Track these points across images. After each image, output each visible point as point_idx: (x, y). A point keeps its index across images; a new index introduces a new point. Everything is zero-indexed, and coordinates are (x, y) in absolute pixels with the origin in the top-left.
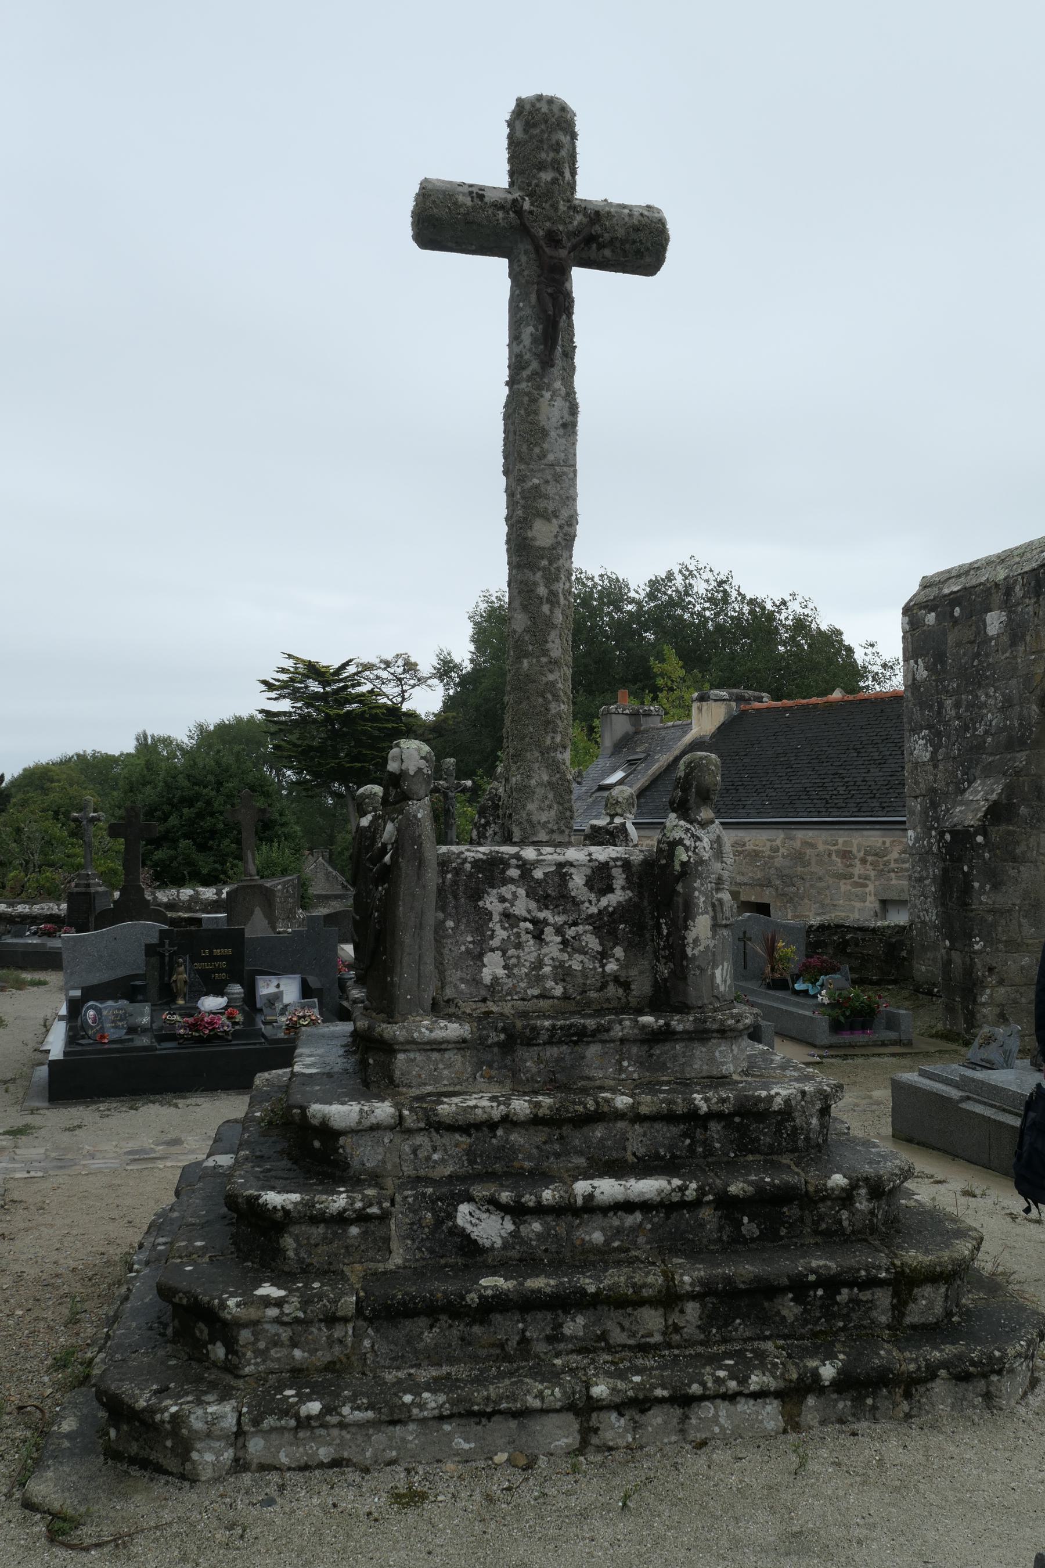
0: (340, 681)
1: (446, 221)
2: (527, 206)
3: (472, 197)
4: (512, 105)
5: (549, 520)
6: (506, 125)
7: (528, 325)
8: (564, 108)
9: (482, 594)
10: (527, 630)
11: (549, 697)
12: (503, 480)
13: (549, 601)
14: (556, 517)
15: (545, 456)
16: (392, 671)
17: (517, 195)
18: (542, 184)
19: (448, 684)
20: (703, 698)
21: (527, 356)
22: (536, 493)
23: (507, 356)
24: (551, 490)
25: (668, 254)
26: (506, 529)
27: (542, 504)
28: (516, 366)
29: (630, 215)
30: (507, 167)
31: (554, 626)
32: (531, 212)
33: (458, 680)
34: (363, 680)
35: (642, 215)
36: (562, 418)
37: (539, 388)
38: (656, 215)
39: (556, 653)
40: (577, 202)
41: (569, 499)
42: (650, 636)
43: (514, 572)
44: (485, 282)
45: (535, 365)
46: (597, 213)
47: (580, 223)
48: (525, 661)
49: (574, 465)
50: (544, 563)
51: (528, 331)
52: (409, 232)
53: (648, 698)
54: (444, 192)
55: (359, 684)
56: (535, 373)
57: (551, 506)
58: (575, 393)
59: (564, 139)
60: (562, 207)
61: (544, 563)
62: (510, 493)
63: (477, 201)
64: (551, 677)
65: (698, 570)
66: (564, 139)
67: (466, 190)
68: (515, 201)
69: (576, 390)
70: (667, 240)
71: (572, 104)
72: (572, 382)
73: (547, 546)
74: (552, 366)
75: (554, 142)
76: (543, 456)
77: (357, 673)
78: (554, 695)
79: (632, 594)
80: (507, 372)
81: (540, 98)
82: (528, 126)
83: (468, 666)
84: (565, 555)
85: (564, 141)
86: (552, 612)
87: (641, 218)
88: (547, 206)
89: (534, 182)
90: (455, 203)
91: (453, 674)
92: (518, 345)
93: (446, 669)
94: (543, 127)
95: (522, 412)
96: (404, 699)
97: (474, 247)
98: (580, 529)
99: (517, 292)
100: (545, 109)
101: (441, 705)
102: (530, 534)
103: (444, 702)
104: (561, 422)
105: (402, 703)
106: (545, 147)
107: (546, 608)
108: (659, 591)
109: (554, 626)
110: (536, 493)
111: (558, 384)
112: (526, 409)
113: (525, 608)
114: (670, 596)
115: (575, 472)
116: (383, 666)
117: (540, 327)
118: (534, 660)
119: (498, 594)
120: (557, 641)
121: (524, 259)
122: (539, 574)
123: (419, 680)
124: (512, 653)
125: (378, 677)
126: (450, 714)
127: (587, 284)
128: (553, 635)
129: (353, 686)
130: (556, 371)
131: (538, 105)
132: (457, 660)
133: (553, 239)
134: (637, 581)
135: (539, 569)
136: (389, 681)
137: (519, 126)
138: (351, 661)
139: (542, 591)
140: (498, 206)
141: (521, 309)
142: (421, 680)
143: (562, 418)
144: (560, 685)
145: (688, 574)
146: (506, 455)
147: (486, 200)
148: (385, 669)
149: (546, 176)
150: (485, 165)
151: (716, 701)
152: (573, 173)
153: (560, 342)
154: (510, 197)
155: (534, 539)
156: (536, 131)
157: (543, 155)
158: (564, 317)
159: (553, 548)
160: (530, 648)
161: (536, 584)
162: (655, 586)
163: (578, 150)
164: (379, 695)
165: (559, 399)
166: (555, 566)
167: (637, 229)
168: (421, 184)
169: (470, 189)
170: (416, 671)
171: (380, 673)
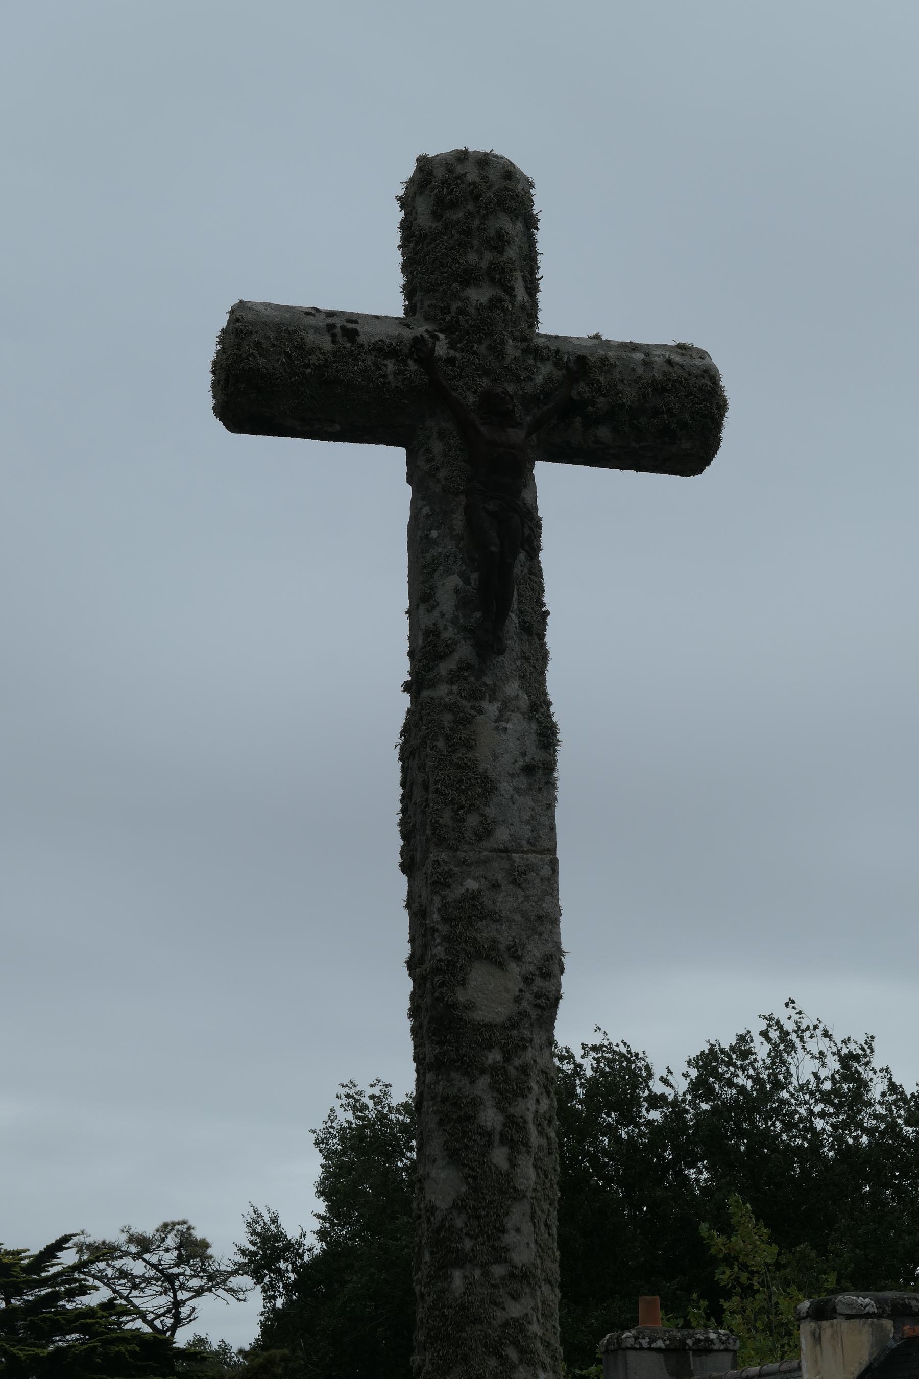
0: (44, 1283)
1: (278, 377)
2: (441, 349)
3: (334, 336)
4: (409, 170)
5: (501, 966)
6: (396, 205)
7: (448, 572)
8: (510, 173)
9: (343, 1091)
10: (458, 1206)
11: (513, 1354)
12: (403, 882)
13: (505, 1140)
14: (518, 958)
15: (489, 833)
16: (154, 1260)
17: (421, 329)
18: (472, 310)
19: (272, 1286)
20: (822, 1313)
21: (449, 634)
22: (473, 909)
23: (407, 632)
24: (505, 901)
25: (725, 434)
26: (408, 985)
27: (486, 932)
28: (426, 652)
29: (647, 364)
30: (400, 280)
31: (519, 1196)
32: (451, 361)
33: (293, 1276)
34: (91, 1281)
35: (669, 362)
36: (524, 754)
37: (475, 696)
38: (698, 362)
39: (523, 1256)
40: (541, 341)
41: (546, 920)
42: (699, 1175)
43: (429, 1077)
44: (359, 495)
45: (464, 650)
46: (582, 360)
47: (549, 379)
48: (457, 1274)
49: (552, 850)
50: (494, 1056)
51: (449, 585)
52: (208, 401)
53: (696, 1313)
54: (278, 327)
55: (83, 1290)
56: (465, 666)
57: (505, 936)
58: (549, 704)
59: (513, 229)
60: (512, 350)
61: (494, 1056)
62: (417, 908)
63: (342, 341)
64: (515, 1310)
65: (800, 1031)
66: (513, 229)
67: (321, 322)
68: (417, 341)
69: (551, 698)
70: (721, 407)
71: (525, 165)
72: (542, 682)
73: (499, 1020)
74: (501, 652)
75: (492, 233)
76: (485, 831)
77: (79, 1267)
78: (522, 1351)
79: (658, 1088)
80: (406, 664)
81: (462, 156)
82: (441, 206)
83: (314, 1245)
84: (539, 1039)
85: (512, 232)
86: (513, 1164)
87: (667, 368)
88: (482, 349)
89: (454, 306)
90: (301, 347)
91: (282, 1265)
92: (429, 611)
93: (268, 1251)
94: (470, 207)
95: (441, 744)
96: (178, 1322)
97: (337, 427)
98: (568, 983)
99: (426, 510)
100: (473, 175)
101: (256, 1332)
102: (461, 997)
103: (263, 1325)
104: (521, 762)
105: (174, 1328)
106: (476, 243)
107: (499, 1156)
108: (719, 1077)
109: (519, 1196)
110: (473, 909)
111: (513, 688)
112: (448, 739)
113: (454, 1156)
114: (742, 1089)
115: (554, 863)
116: (134, 1249)
117: (474, 576)
118: (477, 1273)
119: (376, 1091)
120: (527, 1227)
121: (437, 447)
122: (484, 1081)
123: (211, 1278)
124: (427, 1257)
125: (123, 1274)
126: (277, 1353)
127: (578, 508)
128: (518, 1215)
129: (70, 1295)
130: (509, 661)
131: (459, 169)
132: (292, 1234)
133: (495, 408)
134: (669, 1060)
135: (483, 1072)
136: (148, 1281)
137: (423, 206)
138: (66, 1239)
139: (490, 1117)
140: (384, 350)
141: (435, 543)
142: (216, 1280)
143: (524, 754)
144: (535, 1328)
145: (784, 1043)
146: (407, 830)
147: (362, 339)
148: (137, 1256)
149: (479, 295)
150: (360, 275)
151: (849, 1317)
152: (532, 288)
153: (515, 606)
154: (408, 334)
155: (470, 1006)
156: (457, 215)
157: (472, 258)
158: (522, 556)
159: (512, 1024)
160: (468, 1244)
161: (476, 1103)
162: (709, 1063)
163: (539, 247)
164: (126, 1313)
165: (516, 717)
166: (517, 1062)
167: (661, 388)
168: (232, 312)
169: (330, 321)
170: (205, 1258)
171: (128, 1264)
